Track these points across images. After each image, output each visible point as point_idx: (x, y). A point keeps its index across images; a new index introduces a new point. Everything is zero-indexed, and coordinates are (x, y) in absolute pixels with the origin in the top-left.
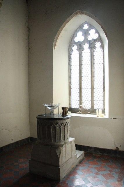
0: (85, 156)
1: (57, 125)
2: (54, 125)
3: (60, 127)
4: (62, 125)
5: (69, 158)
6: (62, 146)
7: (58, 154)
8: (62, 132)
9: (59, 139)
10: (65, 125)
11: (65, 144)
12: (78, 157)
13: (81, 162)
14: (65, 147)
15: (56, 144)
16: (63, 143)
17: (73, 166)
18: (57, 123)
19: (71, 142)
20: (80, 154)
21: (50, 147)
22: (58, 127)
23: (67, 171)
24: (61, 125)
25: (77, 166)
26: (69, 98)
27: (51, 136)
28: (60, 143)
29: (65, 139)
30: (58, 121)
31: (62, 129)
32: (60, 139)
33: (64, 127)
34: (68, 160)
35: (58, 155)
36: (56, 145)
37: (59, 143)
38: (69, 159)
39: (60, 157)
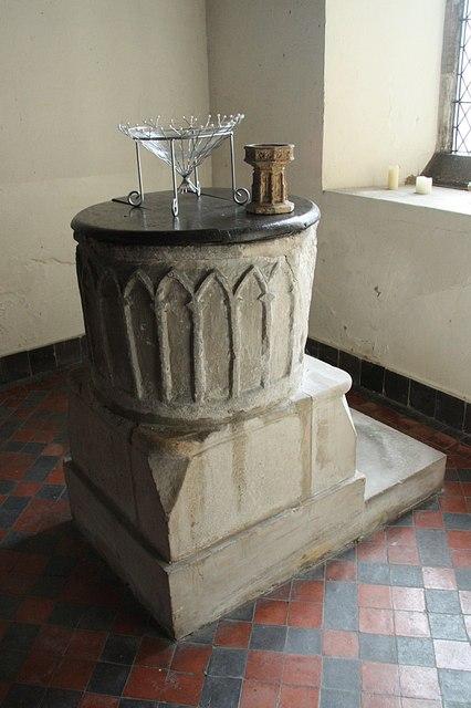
0: (445, 479)
1: (164, 285)
2: (140, 287)
3: (189, 299)
4: (208, 283)
5: (283, 503)
6: (202, 437)
7: (163, 486)
8: (208, 334)
9: (185, 379)
10: (229, 287)
11: (237, 419)
12: (367, 496)
13: (396, 522)
14: (239, 442)
15: (164, 411)
16: (221, 414)
17: (316, 551)
18: (165, 271)
19: (305, 404)
20: (397, 463)
21: (130, 424)
22: (168, 298)
23: (253, 581)
24: (197, 287)
25: (359, 546)
26: (443, 85)
27: (129, 360)
28: (193, 410)
29: (238, 387)
30: (167, 256)
31: (201, 314)
32: (193, 390)
33: (227, 301)
34: (260, 522)
35: (164, 493)
36: (166, 420)
37: (184, 413)
38: (280, 511)
39: (172, 504)
